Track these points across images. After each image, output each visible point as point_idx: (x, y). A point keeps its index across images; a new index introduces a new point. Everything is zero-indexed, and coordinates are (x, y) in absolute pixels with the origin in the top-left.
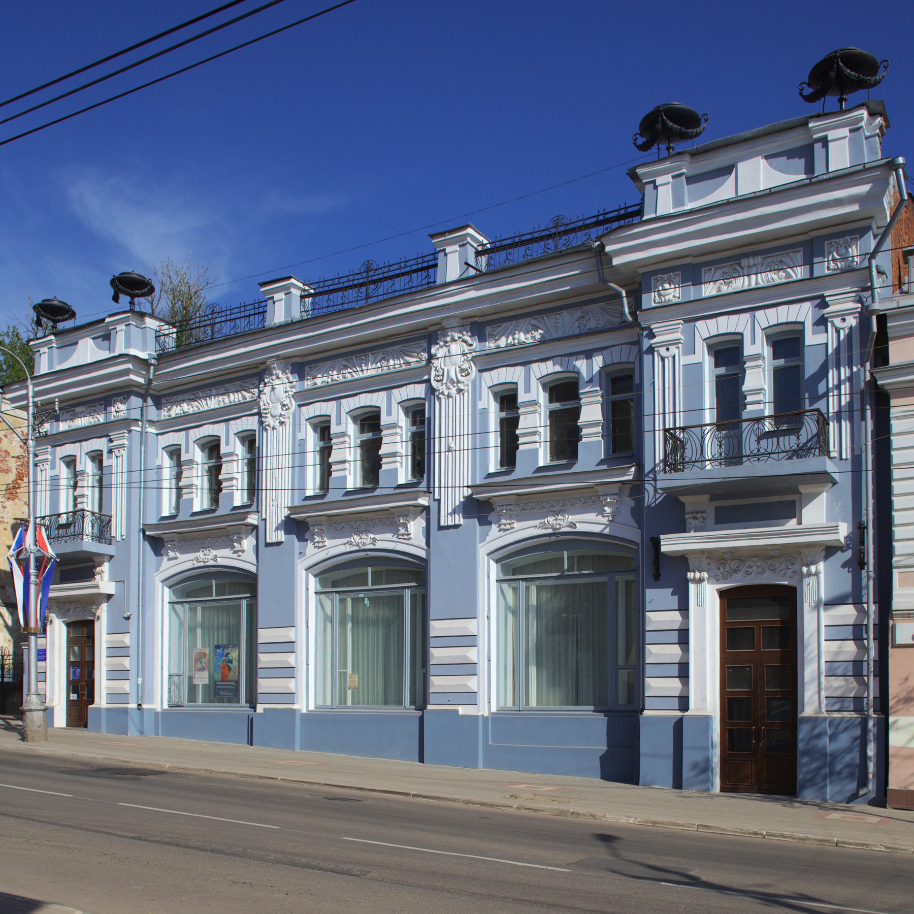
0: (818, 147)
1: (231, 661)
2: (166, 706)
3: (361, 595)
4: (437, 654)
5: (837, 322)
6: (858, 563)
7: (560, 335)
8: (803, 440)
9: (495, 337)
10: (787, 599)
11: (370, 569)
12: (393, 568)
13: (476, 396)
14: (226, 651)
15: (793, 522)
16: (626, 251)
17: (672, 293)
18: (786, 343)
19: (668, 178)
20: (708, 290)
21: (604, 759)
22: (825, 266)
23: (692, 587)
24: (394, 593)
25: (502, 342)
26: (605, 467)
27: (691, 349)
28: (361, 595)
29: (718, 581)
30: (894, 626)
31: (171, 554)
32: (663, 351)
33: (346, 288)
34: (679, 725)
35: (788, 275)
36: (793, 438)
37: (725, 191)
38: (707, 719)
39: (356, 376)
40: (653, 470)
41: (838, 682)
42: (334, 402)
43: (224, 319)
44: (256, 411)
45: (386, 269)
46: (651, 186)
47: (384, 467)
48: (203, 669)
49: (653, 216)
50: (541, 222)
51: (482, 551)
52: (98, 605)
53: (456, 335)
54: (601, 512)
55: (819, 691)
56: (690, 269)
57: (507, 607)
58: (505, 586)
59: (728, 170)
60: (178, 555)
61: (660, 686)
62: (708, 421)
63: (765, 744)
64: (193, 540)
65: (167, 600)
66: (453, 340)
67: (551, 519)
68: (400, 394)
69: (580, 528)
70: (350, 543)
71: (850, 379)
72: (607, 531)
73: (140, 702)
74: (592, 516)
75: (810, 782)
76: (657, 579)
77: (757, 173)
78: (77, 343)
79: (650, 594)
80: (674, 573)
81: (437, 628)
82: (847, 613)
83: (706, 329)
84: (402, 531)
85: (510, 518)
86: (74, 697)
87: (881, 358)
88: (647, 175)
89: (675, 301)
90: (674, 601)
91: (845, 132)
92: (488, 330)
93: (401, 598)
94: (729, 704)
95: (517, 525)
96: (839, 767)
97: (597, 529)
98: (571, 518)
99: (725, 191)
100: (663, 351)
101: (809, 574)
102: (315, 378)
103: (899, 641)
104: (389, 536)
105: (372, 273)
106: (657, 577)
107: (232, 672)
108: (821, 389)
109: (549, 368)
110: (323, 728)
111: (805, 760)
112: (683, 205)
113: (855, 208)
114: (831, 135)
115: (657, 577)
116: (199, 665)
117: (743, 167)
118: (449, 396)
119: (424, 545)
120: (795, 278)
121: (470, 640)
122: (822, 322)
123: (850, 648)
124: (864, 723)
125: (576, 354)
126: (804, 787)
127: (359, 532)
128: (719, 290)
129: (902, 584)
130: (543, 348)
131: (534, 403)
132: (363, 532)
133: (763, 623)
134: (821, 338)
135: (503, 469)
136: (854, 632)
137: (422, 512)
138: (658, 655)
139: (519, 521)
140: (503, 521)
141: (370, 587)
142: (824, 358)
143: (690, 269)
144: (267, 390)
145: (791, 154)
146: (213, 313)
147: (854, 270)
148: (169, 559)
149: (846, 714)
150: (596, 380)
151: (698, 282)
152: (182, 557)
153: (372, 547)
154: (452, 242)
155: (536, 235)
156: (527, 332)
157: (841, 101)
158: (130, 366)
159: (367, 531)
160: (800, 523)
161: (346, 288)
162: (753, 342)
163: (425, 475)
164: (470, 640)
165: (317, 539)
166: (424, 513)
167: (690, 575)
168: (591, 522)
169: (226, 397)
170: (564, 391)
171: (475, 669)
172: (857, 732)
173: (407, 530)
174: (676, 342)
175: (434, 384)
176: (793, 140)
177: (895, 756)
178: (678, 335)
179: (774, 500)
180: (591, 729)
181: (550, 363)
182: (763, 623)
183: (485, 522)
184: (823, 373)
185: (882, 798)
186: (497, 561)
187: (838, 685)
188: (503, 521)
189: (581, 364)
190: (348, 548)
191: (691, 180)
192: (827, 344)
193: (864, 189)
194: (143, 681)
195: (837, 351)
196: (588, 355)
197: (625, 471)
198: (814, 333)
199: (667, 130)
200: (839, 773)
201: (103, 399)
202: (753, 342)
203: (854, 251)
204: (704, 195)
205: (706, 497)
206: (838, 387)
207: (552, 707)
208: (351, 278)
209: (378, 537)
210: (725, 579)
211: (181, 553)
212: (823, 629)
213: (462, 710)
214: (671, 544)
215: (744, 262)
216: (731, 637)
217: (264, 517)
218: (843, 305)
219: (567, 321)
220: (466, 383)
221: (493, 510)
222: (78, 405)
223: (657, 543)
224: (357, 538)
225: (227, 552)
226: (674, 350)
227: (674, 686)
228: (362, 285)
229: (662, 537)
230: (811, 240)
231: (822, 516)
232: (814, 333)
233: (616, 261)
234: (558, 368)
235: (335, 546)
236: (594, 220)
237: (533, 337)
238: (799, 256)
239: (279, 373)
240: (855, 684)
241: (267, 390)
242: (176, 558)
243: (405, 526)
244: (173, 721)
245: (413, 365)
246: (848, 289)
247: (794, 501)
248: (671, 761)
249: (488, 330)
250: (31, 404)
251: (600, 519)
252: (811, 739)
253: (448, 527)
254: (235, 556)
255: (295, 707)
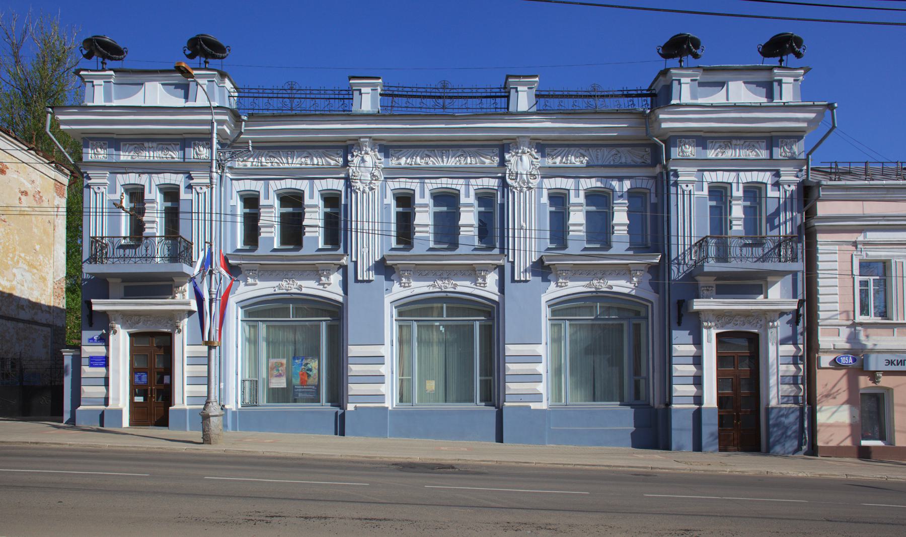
0: (775, 84)
1: (310, 370)
2: (240, 406)
3: (437, 324)
4: (354, 369)
5: (786, 187)
6: (795, 321)
7: (600, 163)
8: (766, 251)
9: (553, 156)
10: (754, 342)
11: (445, 305)
12: (455, 305)
13: (384, 195)
14: (304, 362)
15: (762, 296)
16: (668, 121)
17: (690, 151)
18: (754, 192)
19: (688, 80)
20: (711, 154)
21: (633, 434)
22: (778, 153)
23: (705, 331)
24: (470, 323)
25: (403, 161)
26: (631, 253)
27: (113, 190)
28: (437, 324)
29: (718, 328)
30: (819, 358)
31: (250, 281)
32: (684, 186)
33: (425, 97)
34: (102, 415)
35: (757, 155)
36: (760, 249)
37: (719, 98)
38: (119, 412)
39: (282, 166)
40: (677, 258)
41: (786, 387)
42: (262, 182)
43: (304, 96)
44: (343, 175)
45: (308, 92)
46: (194, 83)
47: (263, 235)
48: (280, 375)
49: (678, 102)
50: (584, 86)
51: (388, 299)
52: (181, 319)
53: (526, 149)
54: (630, 281)
55: (776, 392)
56: (702, 139)
57: (246, 339)
58: (245, 324)
59: (722, 84)
60: (257, 281)
61: (682, 390)
62: (123, 235)
63: (743, 422)
64: (272, 271)
65: (240, 318)
66: (523, 153)
67: (595, 282)
68: (321, 185)
69: (615, 289)
70: (434, 286)
71: (792, 219)
72: (633, 293)
73: (222, 403)
74: (623, 282)
75: (777, 442)
76: (680, 325)
77: (155, 93)
78: (142, 84)
79: (675, 333)
80: (102, 323)
81: (353, 350)
82: (789, 349)
83: (711, 177)
84: (480, 281)
85: (565, 279)
86: (139, 399)
87: (810, 213)
88: (676, 75)
89: (692, 157)
90: (690, 339)
91: (791, 80)
92: (547, 150)
93: (318, 328)
94: (721, 400)
95: (570, 284)
96: (789, 433)
97: (626, 291)
98: (610, 283)
99: (719, 98)
100: (198, 188)
101: (773, 327)
102: (398, 159)
103: (822, 366)
104: (468, 283)
105: (294, 91)
106: (679, 323)
107: (311, 379)
108: (776, 223)
109: (594, 183)
110: (407, 421)
111: (775, 429)
112: (111, 101)
113: (805, 125)
114: (785, 80)
115: (679, 323)
116: (275, 373)
117: (732, 85)
118: (364, 192)
119: (341, 292)
120: (761, 157)
121: (379, 360)
122: (777, 185)
123: (792, 368)
124: (802, 410)
125: (613, 178)
126: (774, 445)
127: (442, 279)
128: (717, 155)
129: (823, 335)
130: (591, 169)
131: (271, 207)
132: (445, 279)
133: (742, 354)
134: (189, 196)
135: (247, 247)
136: (793, 360)
137: (339, 269)
138: (681, 371)
139: (571, 281)
140: (561, 280)
141: (445, 318)
142: (777, 206)
143: (702, 139)
144: (356, 160)
145: (759, 84)
146: (291, 89)
147: (795, 159)
148: (246, 285)
149: (789, 406)
150: (626, 196)
151: (705, 147)
152: (260, 284)
153: (452, 290)
154: (523, 84)
155: (580, 93)
156: (576, 157)
157: (680, 61)
158: (226, 118)
159: (448, 278)
160: (766, 297)
161: (425, 97)
162: (150, 192)
163: (342, 245)
164: (379, 360)
165: (404, 280)
166: (341, 270)
167: (705, 324)
168: (622, 286)
169: (462, 159)
170: (600, 201)
171: (384, 380)
172: (798, 413)
173: (484, 280)
174: (692, 182)
175: (508, 181)
176: (762, 77)
177: (822, 425)
178: (105, 181)
179: (750, 284)
180: (623, 418)
181: (593, 180)
182: (742, 354)
183: (546, 280)
184: (777, 213)
185: (813, 450)
186: (242, 308)
187: (787, 389)
188: (561, 280)
189: (615, 184)
190: (432, 290)
191: (701, 84)
192: (779, 198)
193: (812, 115)
194: (225, 386)
195: (785, 202)
196: (621, 179)
197: (655, 257)
198: (186, 193)
199: (103, 51)
200: (790, 436)
201: (184, 141)
202: (150, 192)
203: (795, 149)
204: (706, 96)
205: (119, 280)
206: (785, 223)
207: (579, 403)
208: (415, 90)
209: (458, 283)
210: (131, 327)
211: (260, 281)
212: (185, 359)
213: (534, 406)
214: (98, 305)
215: (734, 142)
216: (721, 360)
217: (354, 259)
218: (790, 176)
219: (606, 155)
220: (377, 185)
221: (241, 273)
222: (148, 140)
223: (90, 305)
224: (440, 283)
225: (312, 283)
226: (102, 189)
227: (692, 390)
228: (440, 97)
229: (92, 300)
230: (771, 137)
231: (778, 295)
232: (186, 193)
233: (664, 125)
234: (599, 184)
235: (264, 288)
236: (621, 93)
237: (582, 162)
238: (764, 144)
239: (369, 149)
240: (794, 388)
241: (356, 160)
242: (255, 284)
243: (484, 278)
244: (246, 418)
245: (486, 165)
246: (791, 169)
247: (761, 285)
248: (691, 433)
249: (391, 151)
250: (215, 131)
251: (628, 284)
252: (778, 417)
253: (363, 281)
254: (321, 287)
255: (386, 405)
